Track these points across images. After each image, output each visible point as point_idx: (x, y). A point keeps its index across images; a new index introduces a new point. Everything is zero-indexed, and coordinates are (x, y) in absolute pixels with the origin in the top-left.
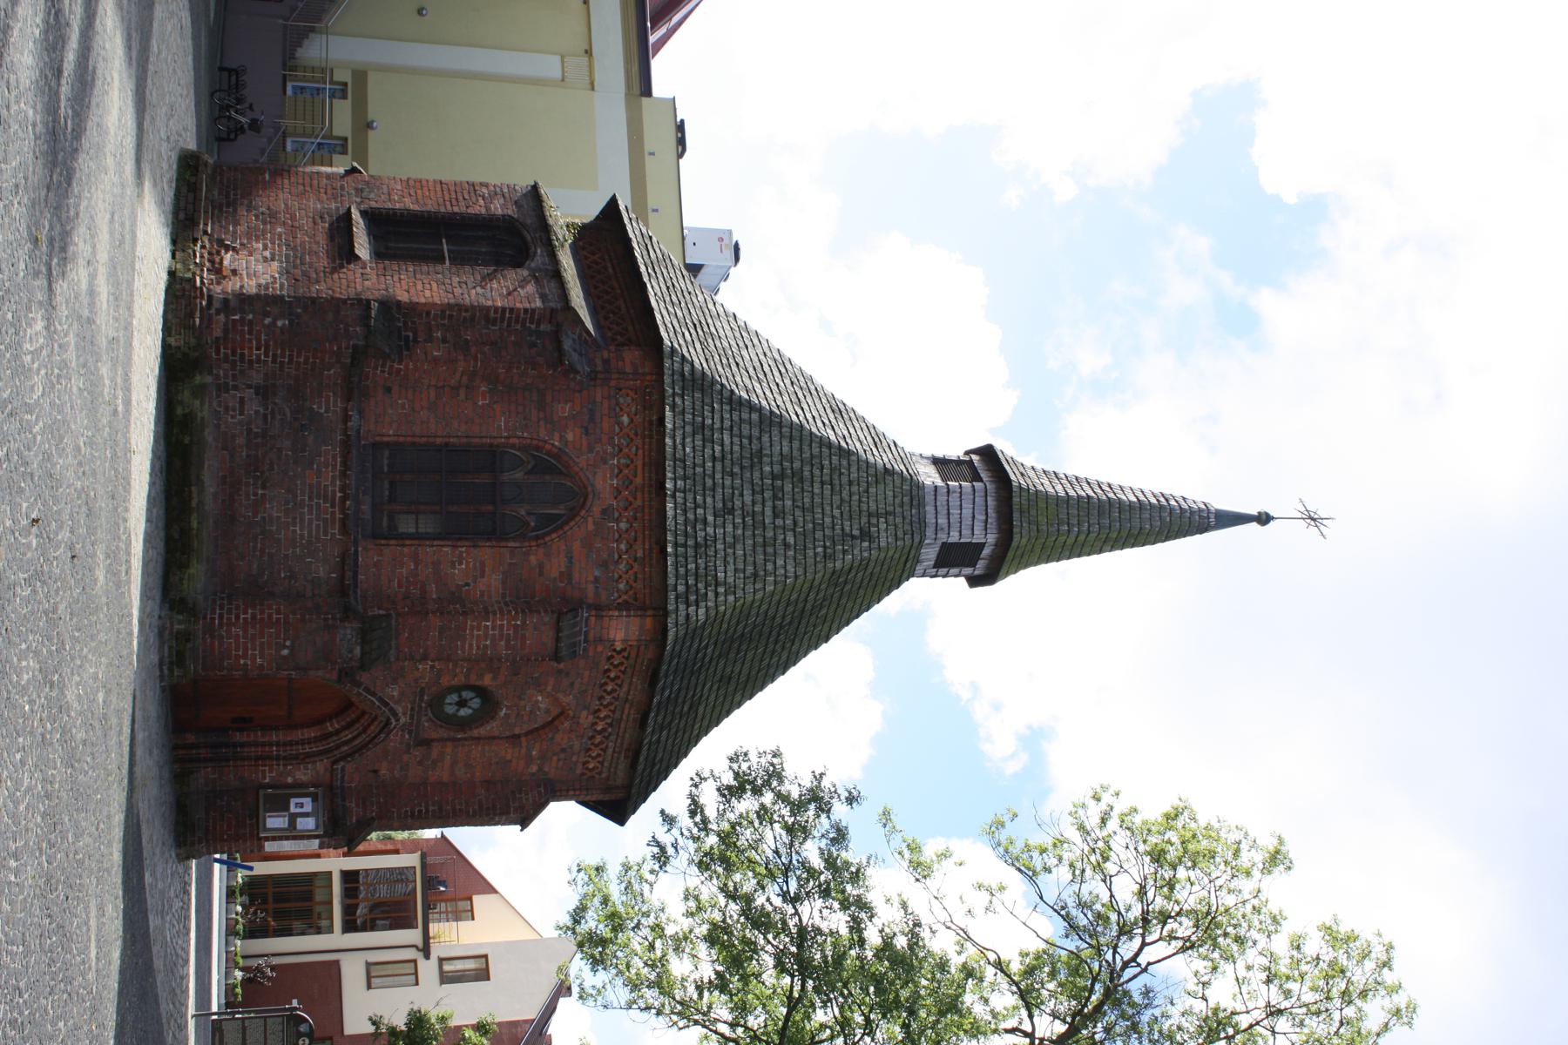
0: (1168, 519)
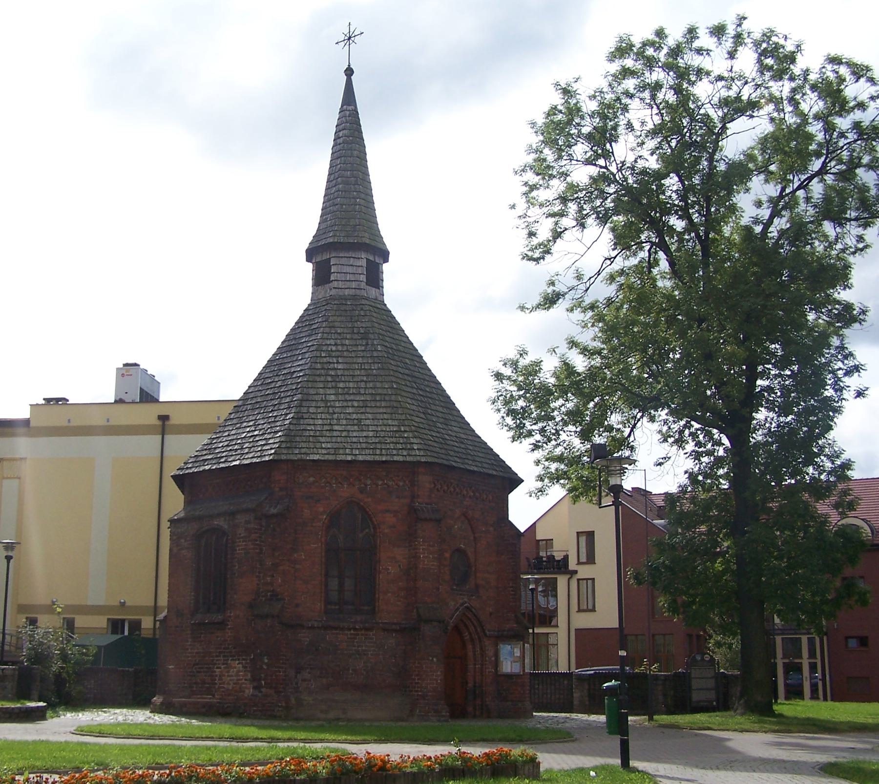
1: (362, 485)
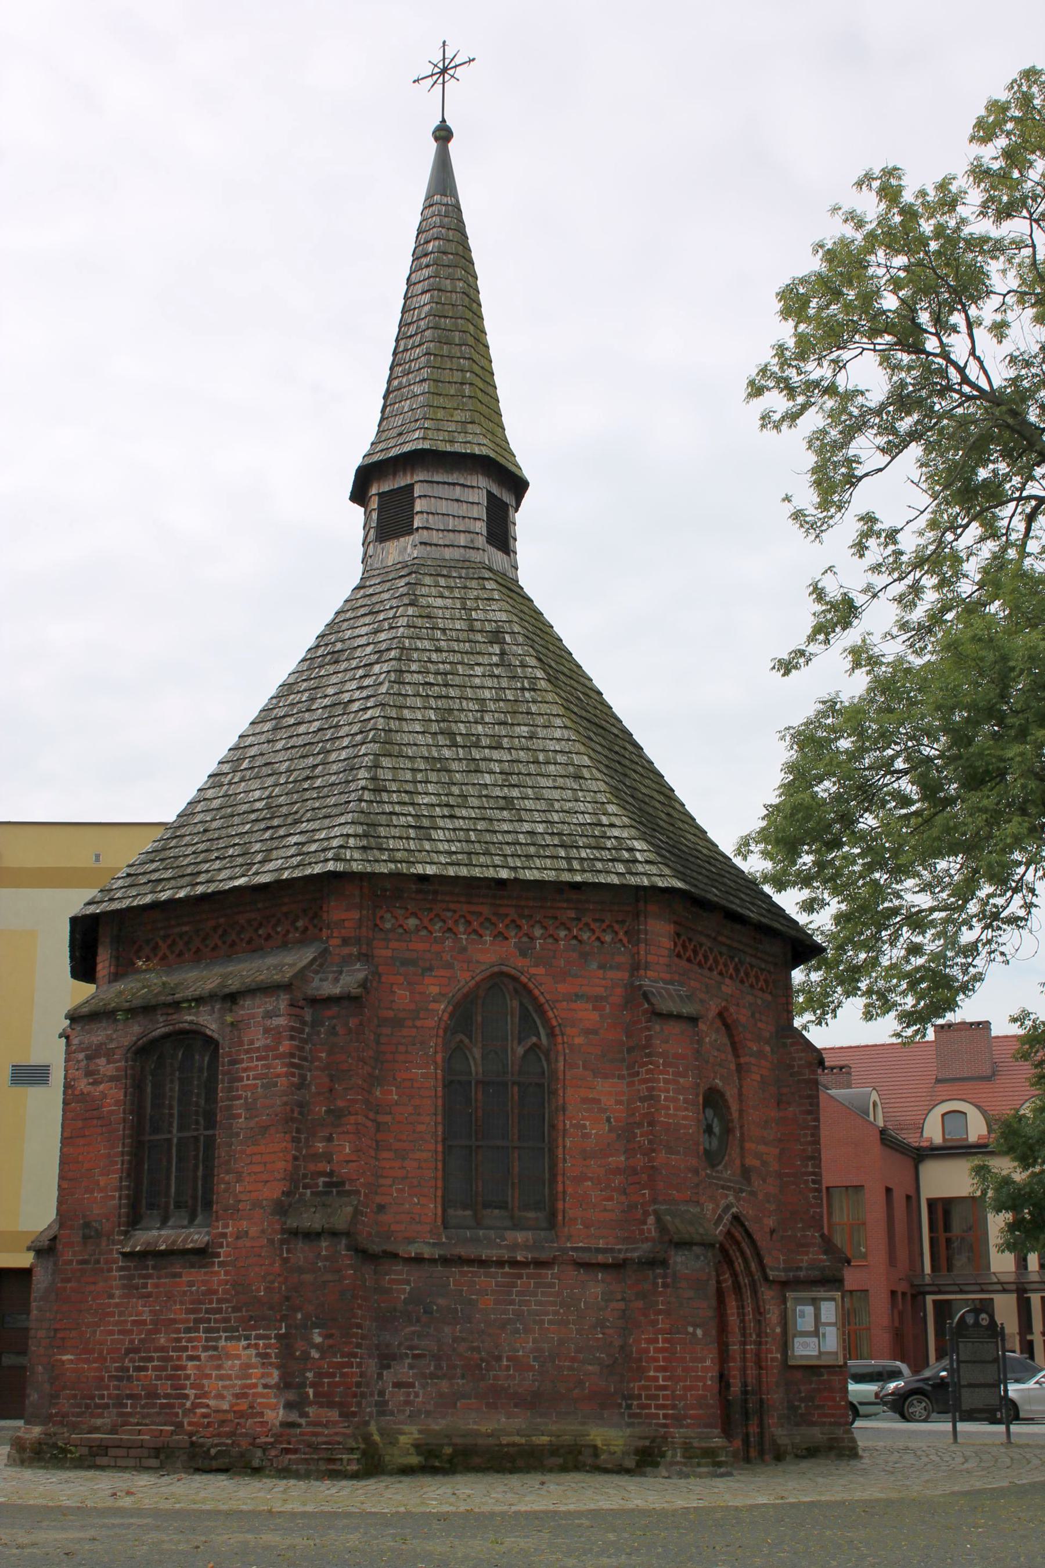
0: (451, 257)
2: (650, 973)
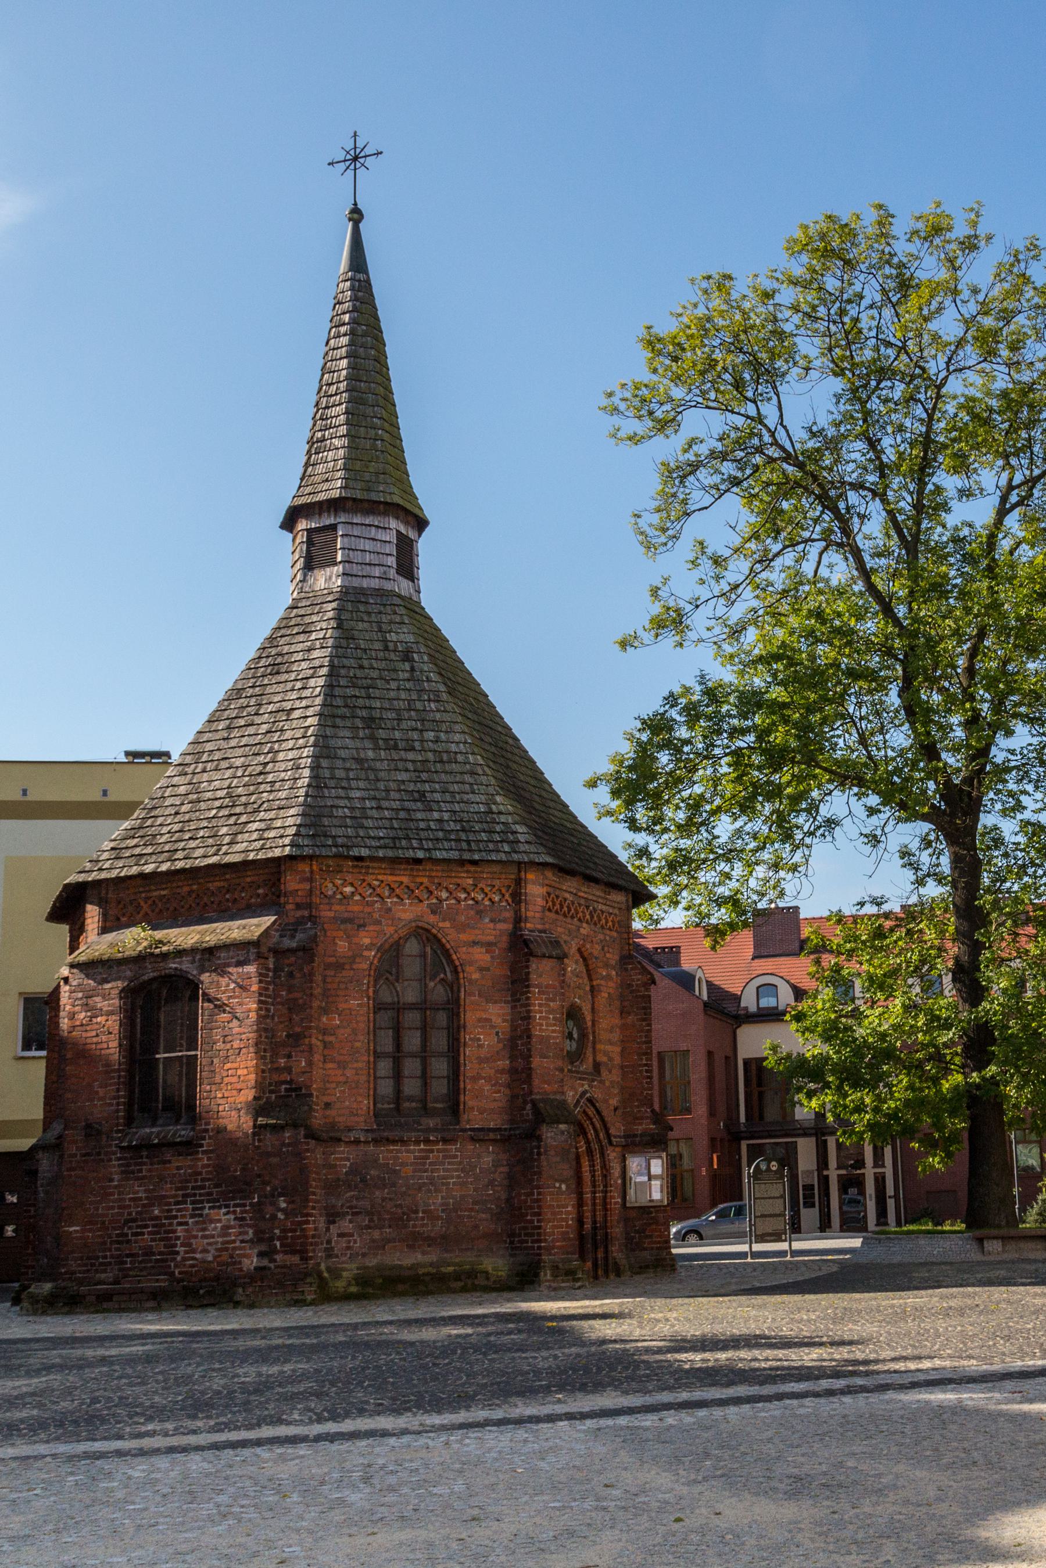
1: (434, 901)
2: (528, 925)
